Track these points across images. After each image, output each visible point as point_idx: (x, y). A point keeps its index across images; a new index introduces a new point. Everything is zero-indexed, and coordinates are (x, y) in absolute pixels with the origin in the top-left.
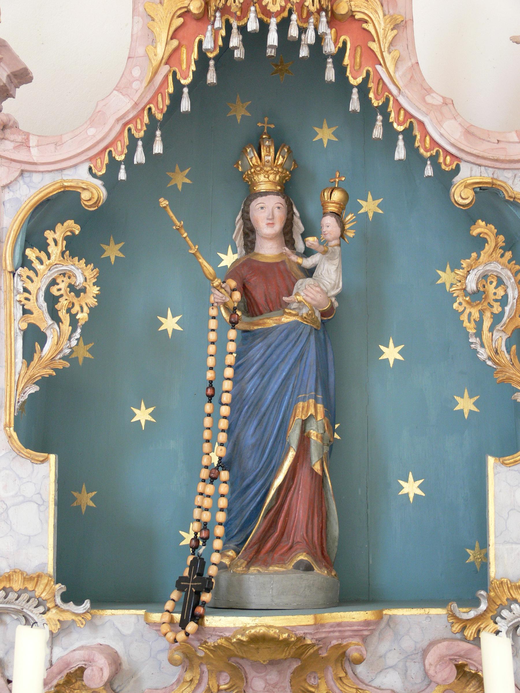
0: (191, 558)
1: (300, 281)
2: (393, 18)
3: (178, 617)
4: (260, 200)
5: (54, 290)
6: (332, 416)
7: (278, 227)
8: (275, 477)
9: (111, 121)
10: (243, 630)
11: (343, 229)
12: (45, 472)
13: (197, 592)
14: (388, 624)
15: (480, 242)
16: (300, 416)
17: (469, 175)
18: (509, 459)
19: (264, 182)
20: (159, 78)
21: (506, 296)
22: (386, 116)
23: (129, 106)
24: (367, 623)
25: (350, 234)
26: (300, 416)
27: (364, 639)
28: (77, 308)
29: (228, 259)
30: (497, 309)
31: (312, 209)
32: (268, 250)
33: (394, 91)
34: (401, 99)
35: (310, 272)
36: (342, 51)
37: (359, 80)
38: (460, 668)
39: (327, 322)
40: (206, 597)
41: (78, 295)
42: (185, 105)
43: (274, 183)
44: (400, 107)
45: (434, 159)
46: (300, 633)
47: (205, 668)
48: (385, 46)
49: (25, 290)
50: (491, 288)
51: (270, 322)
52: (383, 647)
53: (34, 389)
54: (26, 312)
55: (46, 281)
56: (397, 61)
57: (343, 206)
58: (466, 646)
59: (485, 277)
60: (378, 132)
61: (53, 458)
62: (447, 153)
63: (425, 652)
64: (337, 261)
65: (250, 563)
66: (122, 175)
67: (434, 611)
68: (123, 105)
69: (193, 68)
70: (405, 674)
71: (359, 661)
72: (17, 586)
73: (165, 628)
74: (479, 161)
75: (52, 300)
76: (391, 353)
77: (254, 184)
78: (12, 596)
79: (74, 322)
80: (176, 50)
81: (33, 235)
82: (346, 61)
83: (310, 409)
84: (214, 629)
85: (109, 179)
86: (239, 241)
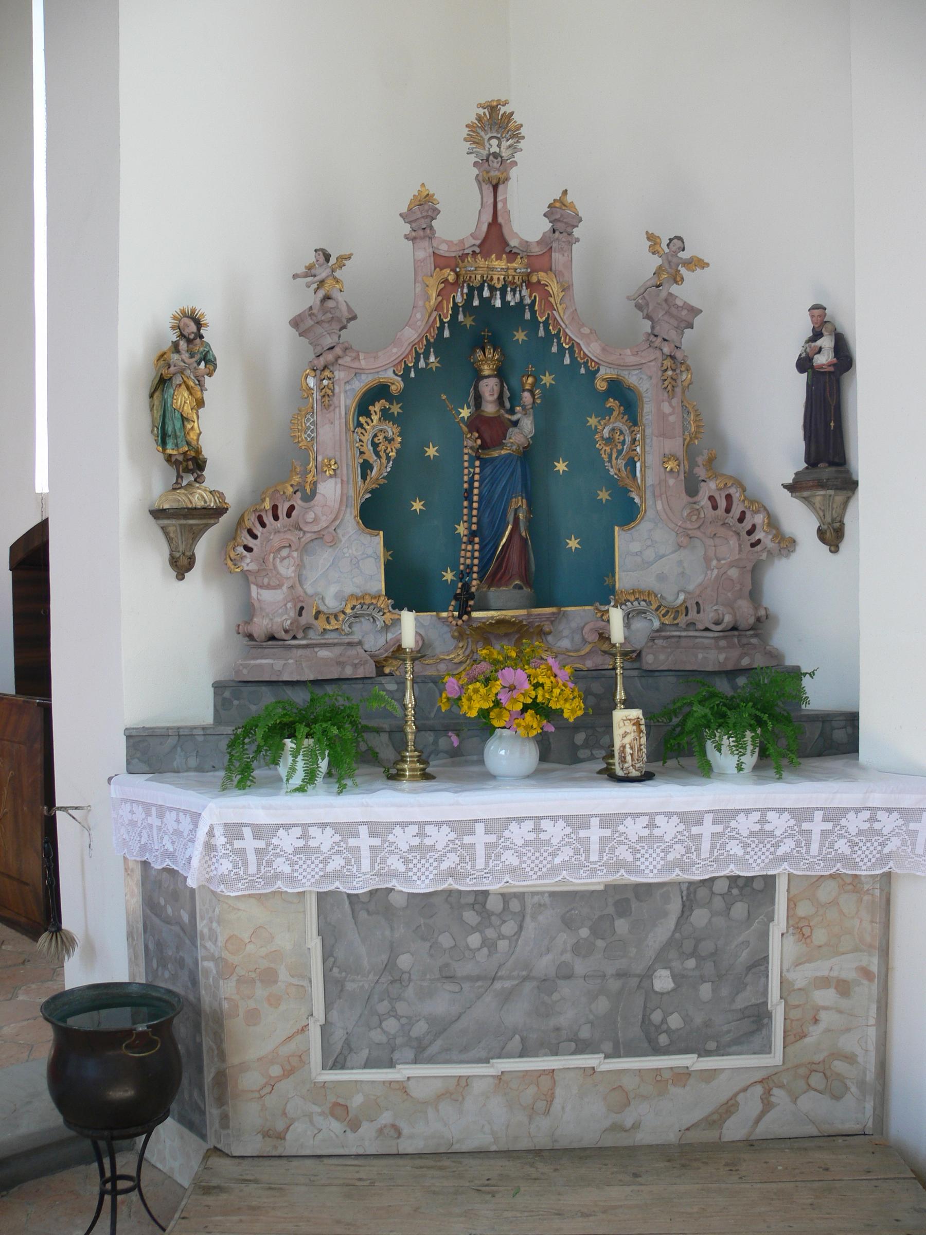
0: (460, 585)
1: (511, 430)
2: (562, 286)
3: (456, 614)
4: (485, 380)
5: (376, 440)
6: (529, 505)
7: (496, 396)
8: (501, 540)
9: (406, 344)
10: (492, 618)
11: (534, 399)
12: (379, 539)
13: (465, 601)
14: (563, 615)
15: (610, 411)
16: (513, 507)
17: (605, 373)
18: (626, 528)
19: (487, 370)
20: (432, 319)
21: (624, 440)
22: (559, 339)
23: (416, 336)
24: (553, 614)
25: (538, 401)
26: (513, 507)
27: (552, 622)
28: (389, 449)
29: (465, 413)
30: (620, 447)
31: (514, 382)
32: (490, 408)
33: (564, 326)
34: (567, 331)
35: (515, 424)
36: (534, 302)
37: (544, 319)
38: (601, 635)
39: (526, 454)
40: (471, 603)
41: (390, 443)
42: (447, 334)
43: (493, 370)
44: (566, 335)
45: (586, 363)
46: (521, 619)
47: (470, 640)
48: (558, 301)
49: (360, 440)
50: (617, 436)
51: (495, 454)
52: (561, 627)
53: (368, 496)
54: (362, 453)
55: (371, 435)
56: (565, 310)
57: (534, 385)
58: (604, 623)
59: (613, 430)
60: (554, 349)
61: (381, 533)
62: (592, 360)
63: (583, 628)
64: (531, 418)
65: (489, 587)
66: (412, 375)
67: (587, 608)
68: (410, 335)
69: (450, 312)
70: (572, 640)
71: (550, 633)
72: (368, 601)
73: (450, 619)
74: (610, 365)
75: (375, 445)
76: (561, 466)
77: (481, 370)
78: (365, 607)
79: (388, 458)
80: (441, 302)
81: (363, 409)
82: (536, 308)
83: (519, 503)
84: (477, 618)
85: (405, 377)
86: (472, 403)
